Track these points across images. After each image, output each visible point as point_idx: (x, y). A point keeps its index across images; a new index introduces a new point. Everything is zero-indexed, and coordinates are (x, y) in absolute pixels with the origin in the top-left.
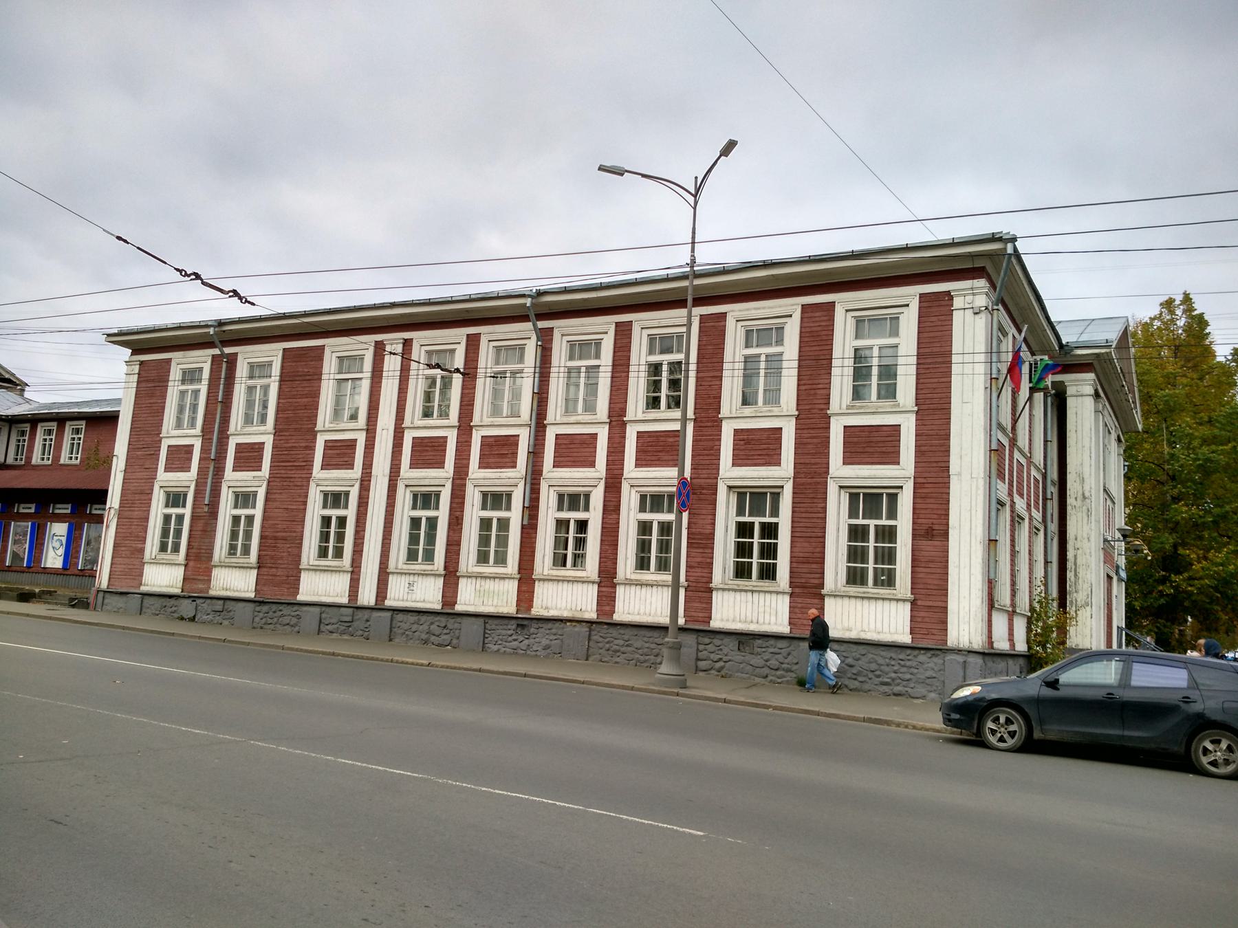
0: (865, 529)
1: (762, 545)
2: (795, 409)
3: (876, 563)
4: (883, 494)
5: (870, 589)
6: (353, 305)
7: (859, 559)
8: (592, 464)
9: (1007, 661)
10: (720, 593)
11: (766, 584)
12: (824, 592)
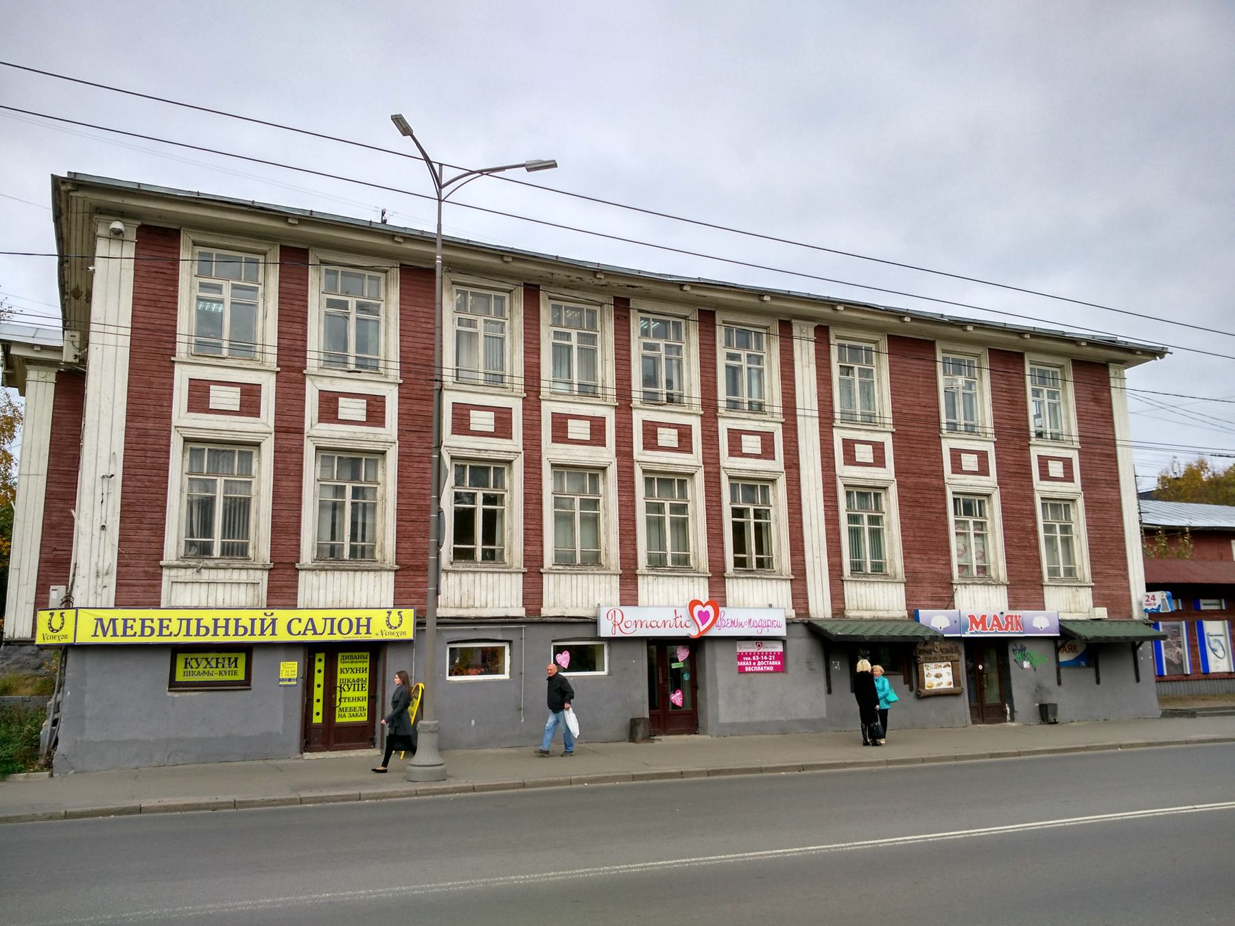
6: (53, 223)
7: (226, 544)
12: (725, 575)
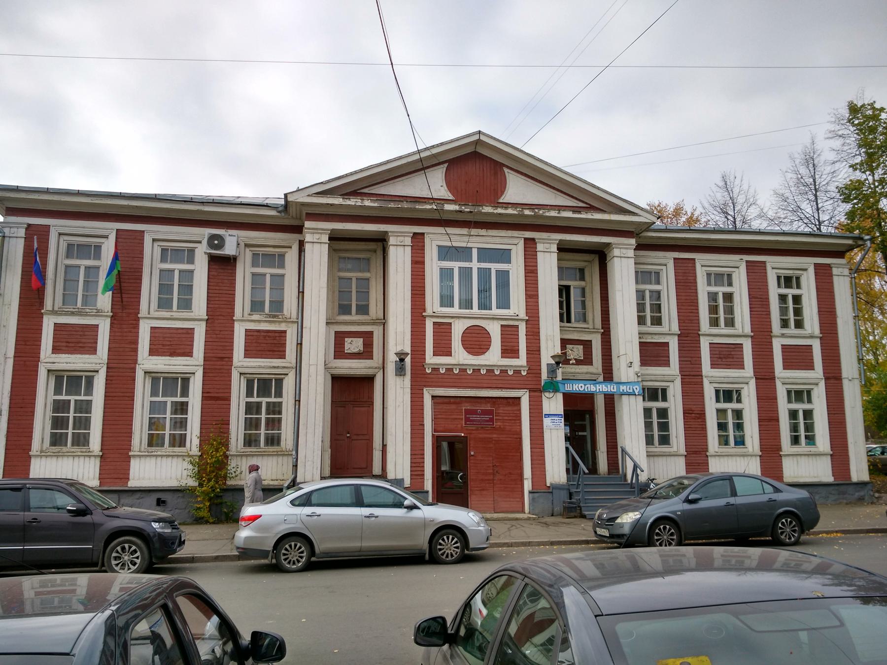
0: (259, 405)
1: (267, 419)
2: (206, 315)
3: (74, 429)
4: (272, 379)
5: (167, 449)
6: (46, 187)
8: (189, 354)
9: (119, 495)
10: (138, 460)
11: (740, 450)
